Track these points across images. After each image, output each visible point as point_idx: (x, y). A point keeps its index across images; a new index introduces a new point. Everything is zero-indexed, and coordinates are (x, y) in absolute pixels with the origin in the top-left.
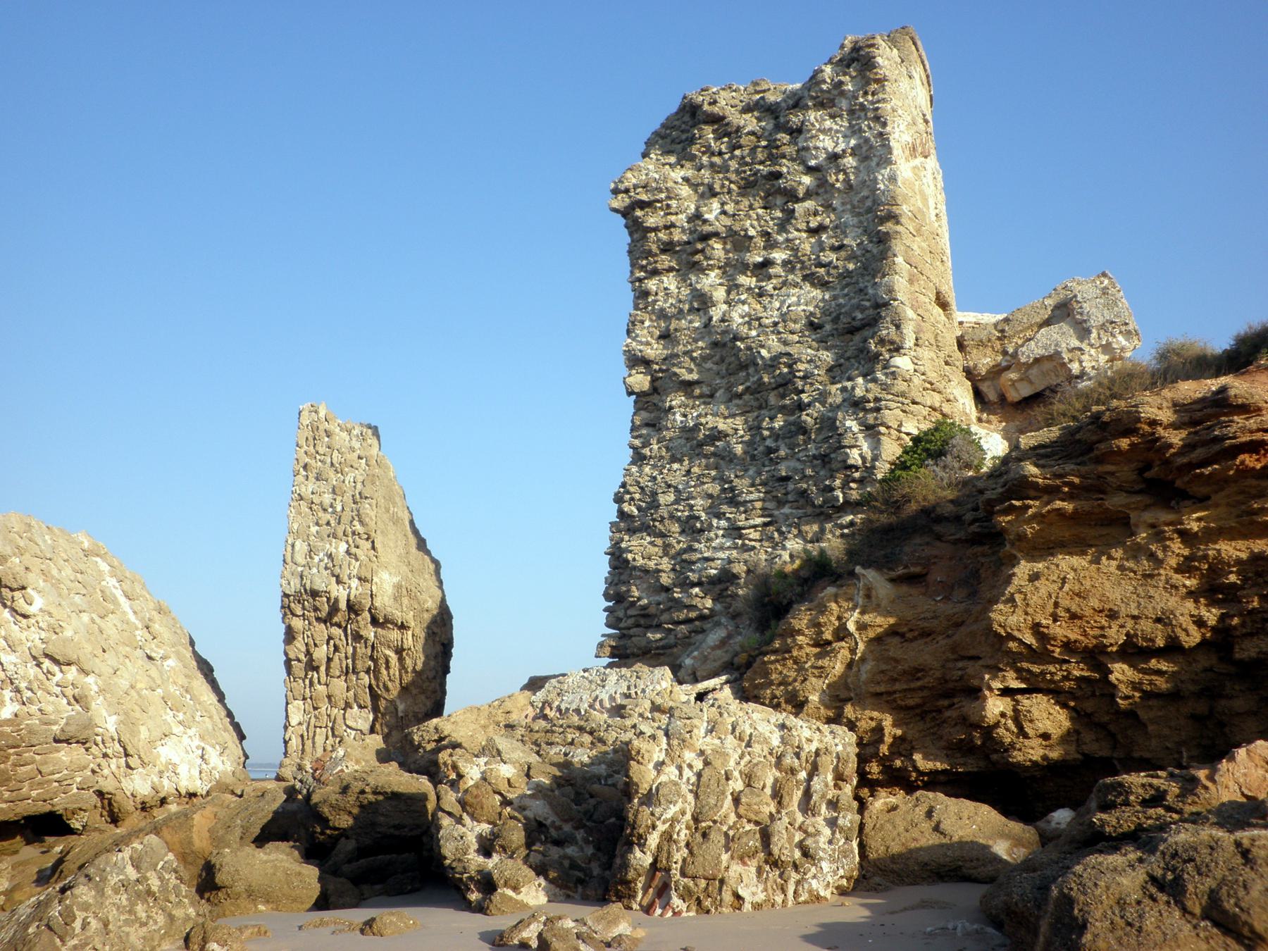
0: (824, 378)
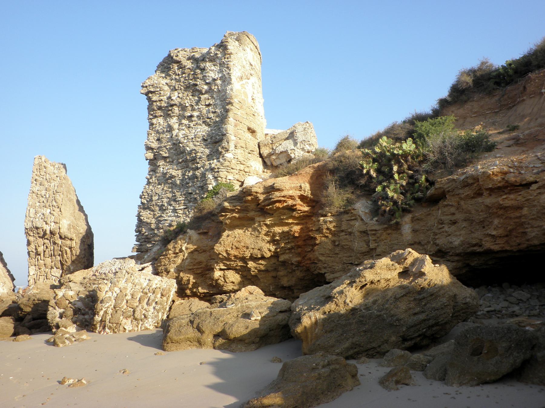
0: (206, 159)
